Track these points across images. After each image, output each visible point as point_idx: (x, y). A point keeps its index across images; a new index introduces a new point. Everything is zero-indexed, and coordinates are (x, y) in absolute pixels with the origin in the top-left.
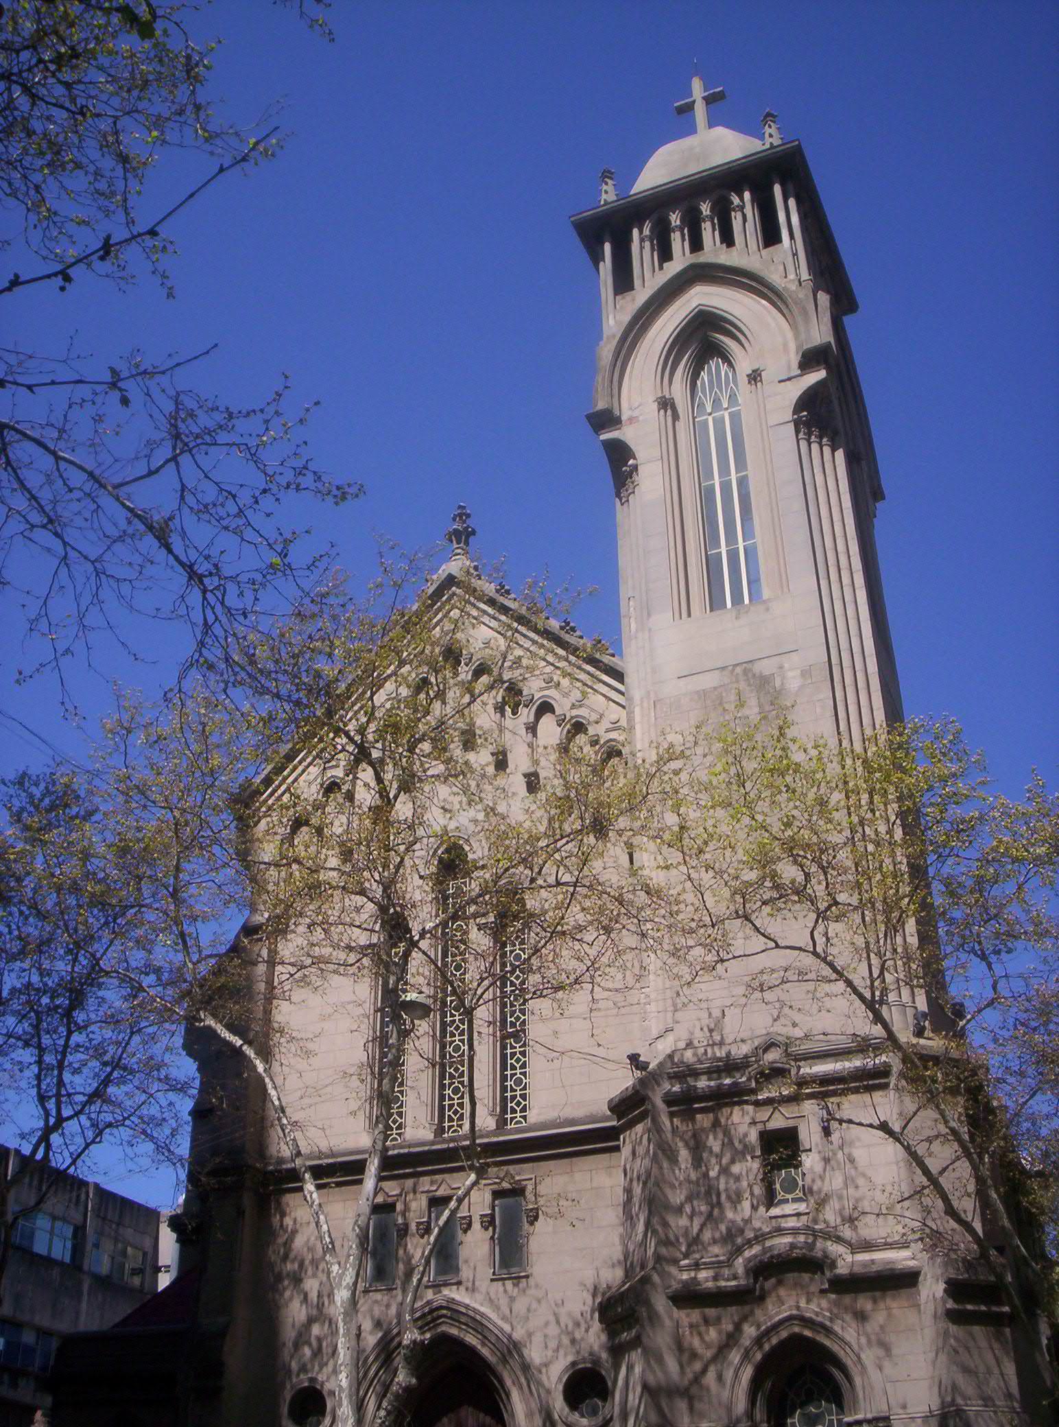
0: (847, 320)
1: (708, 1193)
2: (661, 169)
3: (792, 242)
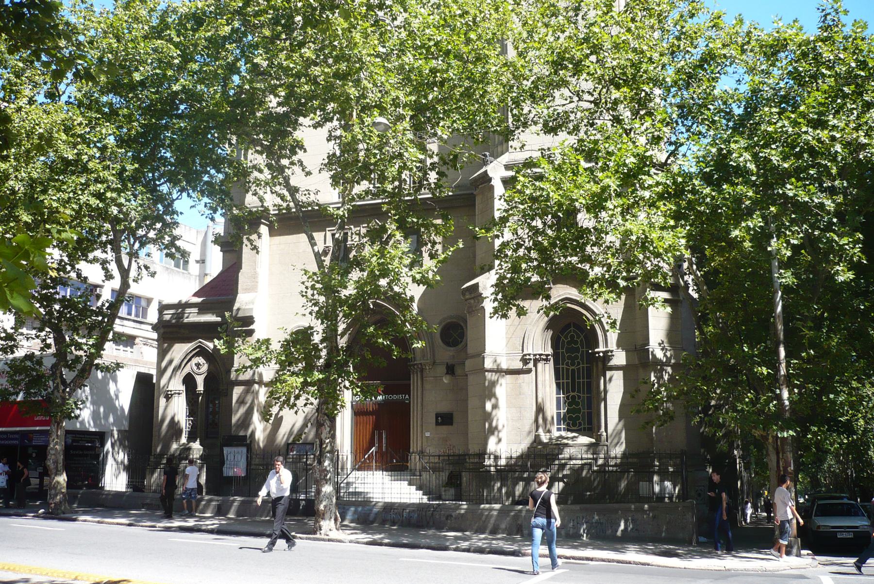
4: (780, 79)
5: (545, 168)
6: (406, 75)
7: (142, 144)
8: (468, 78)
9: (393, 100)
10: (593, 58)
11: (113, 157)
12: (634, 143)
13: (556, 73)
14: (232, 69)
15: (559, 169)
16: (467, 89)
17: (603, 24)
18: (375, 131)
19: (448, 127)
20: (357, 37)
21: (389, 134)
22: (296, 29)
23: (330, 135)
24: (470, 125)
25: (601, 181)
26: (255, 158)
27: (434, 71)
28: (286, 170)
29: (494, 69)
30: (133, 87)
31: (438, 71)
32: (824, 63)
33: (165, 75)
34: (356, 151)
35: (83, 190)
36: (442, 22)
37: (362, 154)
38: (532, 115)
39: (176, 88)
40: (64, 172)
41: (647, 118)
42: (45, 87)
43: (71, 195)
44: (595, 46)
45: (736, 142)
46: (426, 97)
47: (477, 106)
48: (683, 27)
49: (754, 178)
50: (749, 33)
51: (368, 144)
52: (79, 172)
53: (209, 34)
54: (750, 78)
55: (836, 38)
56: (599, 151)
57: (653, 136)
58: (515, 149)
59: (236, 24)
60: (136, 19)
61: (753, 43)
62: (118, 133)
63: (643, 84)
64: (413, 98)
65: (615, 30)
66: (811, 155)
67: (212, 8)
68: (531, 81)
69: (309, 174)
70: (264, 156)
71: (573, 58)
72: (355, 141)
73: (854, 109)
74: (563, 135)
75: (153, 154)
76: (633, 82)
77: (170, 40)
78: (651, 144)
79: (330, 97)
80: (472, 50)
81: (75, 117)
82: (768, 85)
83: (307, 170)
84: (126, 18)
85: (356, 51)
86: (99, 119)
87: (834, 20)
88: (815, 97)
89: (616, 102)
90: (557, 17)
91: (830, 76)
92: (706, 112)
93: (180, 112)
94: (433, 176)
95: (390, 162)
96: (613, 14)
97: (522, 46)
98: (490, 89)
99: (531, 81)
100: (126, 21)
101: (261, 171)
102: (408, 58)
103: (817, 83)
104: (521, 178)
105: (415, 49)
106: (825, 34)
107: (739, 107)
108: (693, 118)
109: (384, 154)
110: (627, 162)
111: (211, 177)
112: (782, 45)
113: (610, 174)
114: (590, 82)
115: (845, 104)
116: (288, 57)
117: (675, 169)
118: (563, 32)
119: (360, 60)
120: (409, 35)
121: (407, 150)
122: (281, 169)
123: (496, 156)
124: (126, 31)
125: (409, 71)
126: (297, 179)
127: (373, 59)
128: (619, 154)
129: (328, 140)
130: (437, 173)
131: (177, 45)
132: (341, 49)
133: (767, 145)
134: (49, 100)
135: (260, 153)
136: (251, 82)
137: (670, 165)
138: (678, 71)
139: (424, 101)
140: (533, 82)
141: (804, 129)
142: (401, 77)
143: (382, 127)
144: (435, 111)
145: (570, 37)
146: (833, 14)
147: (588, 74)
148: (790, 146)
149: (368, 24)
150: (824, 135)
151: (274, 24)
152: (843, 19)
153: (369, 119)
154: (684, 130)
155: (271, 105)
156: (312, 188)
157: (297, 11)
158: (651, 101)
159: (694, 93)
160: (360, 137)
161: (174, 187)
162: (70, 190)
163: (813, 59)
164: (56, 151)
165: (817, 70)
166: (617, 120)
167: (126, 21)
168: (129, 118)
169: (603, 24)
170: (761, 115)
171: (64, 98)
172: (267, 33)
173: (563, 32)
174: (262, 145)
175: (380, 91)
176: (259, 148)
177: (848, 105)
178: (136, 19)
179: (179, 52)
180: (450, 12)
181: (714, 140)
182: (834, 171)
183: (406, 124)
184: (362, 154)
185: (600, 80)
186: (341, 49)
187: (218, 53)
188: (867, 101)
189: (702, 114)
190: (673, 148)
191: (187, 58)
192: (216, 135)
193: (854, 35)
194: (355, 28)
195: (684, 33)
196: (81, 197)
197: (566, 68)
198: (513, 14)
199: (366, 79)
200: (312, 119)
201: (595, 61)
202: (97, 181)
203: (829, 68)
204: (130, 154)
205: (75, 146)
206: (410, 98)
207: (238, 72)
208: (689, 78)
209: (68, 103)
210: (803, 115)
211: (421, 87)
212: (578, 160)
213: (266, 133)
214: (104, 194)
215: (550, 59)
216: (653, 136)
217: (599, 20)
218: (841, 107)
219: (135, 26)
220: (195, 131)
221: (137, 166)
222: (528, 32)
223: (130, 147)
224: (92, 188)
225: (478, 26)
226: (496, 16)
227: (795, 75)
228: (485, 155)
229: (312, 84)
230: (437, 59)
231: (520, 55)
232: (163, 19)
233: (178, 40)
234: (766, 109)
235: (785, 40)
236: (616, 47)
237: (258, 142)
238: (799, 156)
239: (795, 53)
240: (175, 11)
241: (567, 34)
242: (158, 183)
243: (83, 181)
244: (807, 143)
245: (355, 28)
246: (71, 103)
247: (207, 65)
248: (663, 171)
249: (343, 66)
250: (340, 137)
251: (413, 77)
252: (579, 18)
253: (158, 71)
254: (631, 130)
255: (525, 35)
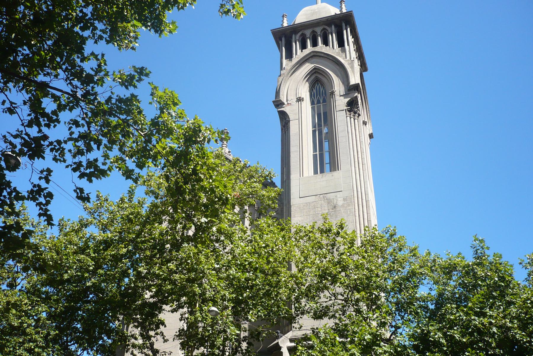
0: (364, 73)
1: (162, 301)
2: (303, 16)
3: (350, 47)
4: (455, 288)
5: (315, 341)
6: (230, 281)
7: (63, 319)
8: (268, 284)
9: (222, 296)
10: (343, 274)
11: (43, 327)
12: (369, 326)
13: (321, 282)
14: (125, 273)
15: (323, 342)
16: (268, 291)
17: (348, 254)
18: (209, 315)
19: (255, 314)
20: (202, 258)
21: (218, 317)
22: (166, 252)
23: (182, 317)
24: (269, 313)
25: (350, 350)
26: (133, 330)
27: (247, 279)
28: (152, 338)
29: (283, 279)
30: (62, 282)
31: (250, 280)
32: (480, 278)
33: (83, 276)
34: (198, 327)
35: (20, 347)
36: (253, 251)
37: (200, 330)
38: (307, 308)
39: (89, 284)
40: (10, 334)
41: (377, 311)
42: (8, 280)
43: (11, 349)
44: (344, 266)
45: (432, 325)
46: (242, 296)
47: (273, 301)
48: (395, 256)
49: (445, 349)
50: (434, 261)
51: (205, 323)
52: (20, 335)
53: (113, 253)
54: (437, 286)
55: (484, 263)
56: (348, 331)
57: (381, 322)
58: (296, 328)
59: (130, 248)
60: (70, 243)
61: (437, 266)
62: (49, 311)
63: (374, 289)
64: (234, 296)
65: (356, 257)
66: (478, 334)
67: (117, 238)
68: (306, 286)
69: (166, 341)
70: (139, 329)
71: (331, 273)
72: (196, 321)
73: (500, 305)
74: (326, 320)
75: (68, 327)
76: (367, 287)
77: (88, 255)
78: (380, 327)
79: (184, 293)
80: (271, 267)
81: (23, 300)
82: (448, 291)
83: (165, 338)
84: (64, 241)
85: (200, 266)
86: (38, 301)
87: (482, 253)
88: (475, 298)
89: (358, 300)
90: (321, 249)
91: (484, 286)
92: (412, 307)
93: (89, 299)
94: (244, 345)
95: (218, 335)
96: (355, 248)
97: (300, 266)
98: (281, 291)
99: (306, 286)
100: (64, 243)
101: (136, 339)
102: (233, 271)
103: (477, 290)
104: (300, 348)
105: (236, 266)
106: (478, 261)
107: (432, 304)
108: (405, 310)
109: (214, 330)
110: (366, 338)
111: (104, 341)
112: (454, 267)
113: (354, 346)
114: (341, 288)
115: (495, 302)
116: (160, 268)
117: (396, 342)
118: (325, 258)
119: (203, 272)
120: (233, 258)
121: (229, 328)
122: (149, 338)
123: (284, 333)
124: (63, 249)
125: (233, 279)
126: (158, 345)
127: (210, 271)
128: (360, 333)
129: (181, 320)
130: (247, 343)
131: (93, 259)
132: (192, 264)
133: (451, 328)
134: (9, 289)
135: (137, 327)
136: (135, 282)
137: (392, 340)
138: (394, 282)
139: (240, 298)
140: (307, 287)
141: (473, 317)
142: (227, 283)
143: (214, 313)
144: (247, 304)
145: (329, 261)
146: (481, 249)
147: (340, 283)
148: (466, 327)
149: (209, 251)
150: (485, 321)
151: (153, 248)
152: (487, 252)
153: (206, 308)
154: (400, 318)
155: (146, 296)
156: (168, 351)
157: (167, 242)
158: (379, 300)
159: (402, 297)
160: (200, 319)
161: (79, 347)
162: (11, 346)
163: (473, 275)
164: (8, 320)
165: (476, 282)
166: (358, 311)
167: (64, 243)
168: (57, 301)
169: (348, 254)
170: (446, 309)
171: (19, 287)
172: (148, 253)
173: (325, 258)
174: (138, 322)
175: (214, 291)
176: (136, 324)
177: (497, 303)
178: (70, 243)
179: (93, 263)
180: (258, 245)
181: (418, 325)
182: (494, 345)
183: (229, 312)
184: (200, 330)
185: (347, 287)
186: (192, 264)
187: (117, 264)
188: (508, 301)
189: (410, 308)
190: (393, 329)
191: (98, 266)
192: (110, 314)
193: (495, 262)
194: (201, 253)
195: (397, 260)
196: (18, 351)
197: (327, 279)
198: (296, 248)
199: (206, 283)
200: (171, 306)
201: (344, 275)
202: (30, 341)
203: (482, 281)
204: (54, 324)
205: (20, 317)
206: (232, 295)
207: (128, 276)
208: (399, 287)
209: (20, 290)
210: (471, 309)
211: (239, 289)
212: (335, 337)
213: (141, 314)
214: (34, 349)
215: (318, 274)
216: (381, 322)
217: (346, 251)
218: (493, 304)
219: (69, 246)
220: (97, 312)
221: (57, 332)
222: (304, 257)
223: (55, 320)
224: (26, 345)
225: (275, 254)
226: (285, 248)
227: (463, 285)
228: (277, 333)
229: (173, 285)
230: (249, 272)
231: (300, 271)
232: (86, 242)
233: (94, 255)
234: (449, 305)
235: (455, 264)
236: (357, 267)
237: (136, 320)
238: (471, 334)
239: (462, 272)
240: (94, 239)
241: (327, 259)
242: (69, 344)
243: (21, 341)
244: (475, 326)
245: (201, 253)
246: (23, 291)
247: (110, 271)
248: (388, 344)
249: (193, 275)
250: (187, 318)
251: (234, 283)
252: (335, 250)
253: (79, 274)
254: (367, 318)
255: (302, 259)
